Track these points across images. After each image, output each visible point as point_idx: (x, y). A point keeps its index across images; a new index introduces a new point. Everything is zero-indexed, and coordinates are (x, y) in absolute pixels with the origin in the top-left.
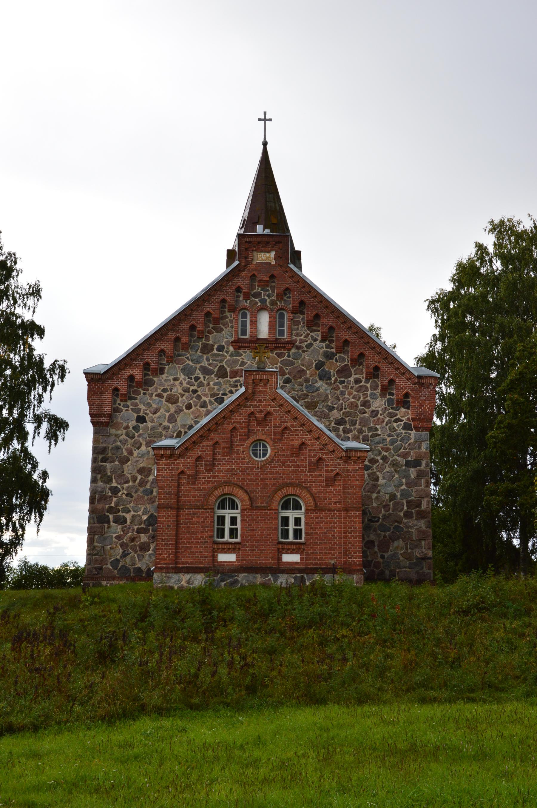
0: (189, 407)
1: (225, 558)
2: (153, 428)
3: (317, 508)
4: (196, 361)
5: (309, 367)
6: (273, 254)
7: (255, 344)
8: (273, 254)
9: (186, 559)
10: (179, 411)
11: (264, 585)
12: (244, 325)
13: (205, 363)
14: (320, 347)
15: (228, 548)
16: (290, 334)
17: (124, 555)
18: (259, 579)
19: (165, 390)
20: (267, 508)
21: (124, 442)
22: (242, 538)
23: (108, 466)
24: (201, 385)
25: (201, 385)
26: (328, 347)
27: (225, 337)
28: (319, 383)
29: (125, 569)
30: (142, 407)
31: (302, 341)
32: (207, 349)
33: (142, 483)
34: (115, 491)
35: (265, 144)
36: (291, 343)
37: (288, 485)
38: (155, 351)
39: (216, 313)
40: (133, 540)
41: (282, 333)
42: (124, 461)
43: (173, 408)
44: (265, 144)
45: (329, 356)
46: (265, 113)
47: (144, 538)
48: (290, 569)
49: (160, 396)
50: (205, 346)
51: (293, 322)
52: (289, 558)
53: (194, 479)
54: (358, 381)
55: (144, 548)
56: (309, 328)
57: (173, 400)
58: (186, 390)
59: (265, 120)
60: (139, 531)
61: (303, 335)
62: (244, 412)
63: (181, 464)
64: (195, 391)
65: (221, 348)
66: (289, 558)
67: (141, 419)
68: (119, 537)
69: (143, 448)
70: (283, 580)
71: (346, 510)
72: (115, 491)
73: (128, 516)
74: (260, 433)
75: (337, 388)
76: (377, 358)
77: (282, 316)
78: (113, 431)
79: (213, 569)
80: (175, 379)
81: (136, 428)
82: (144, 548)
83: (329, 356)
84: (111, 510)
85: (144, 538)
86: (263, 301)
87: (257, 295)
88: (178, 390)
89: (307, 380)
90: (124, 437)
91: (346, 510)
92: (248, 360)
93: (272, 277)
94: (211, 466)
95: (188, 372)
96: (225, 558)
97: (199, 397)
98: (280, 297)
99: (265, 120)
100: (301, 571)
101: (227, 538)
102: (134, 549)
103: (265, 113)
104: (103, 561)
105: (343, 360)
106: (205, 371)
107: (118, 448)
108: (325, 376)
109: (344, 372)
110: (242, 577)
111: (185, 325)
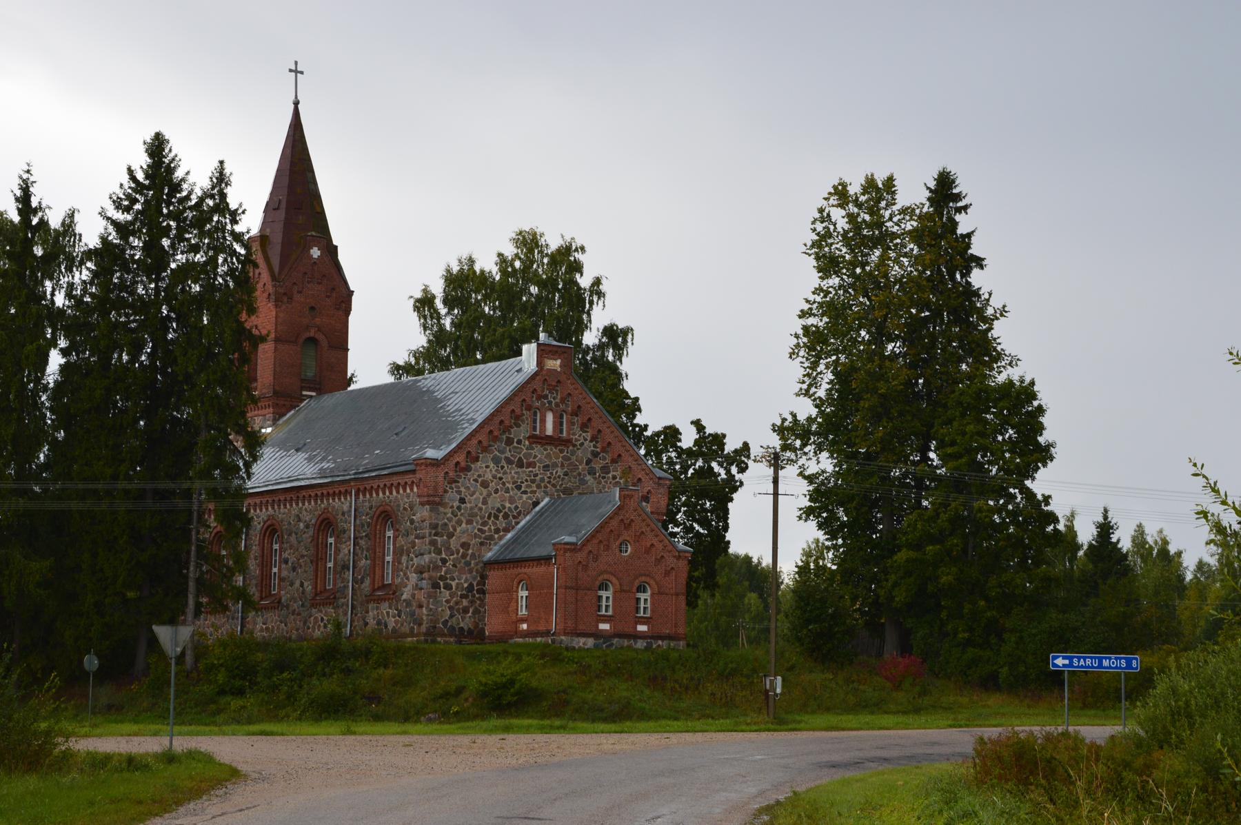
0: (496, 491)
1: (604, 626)
2: (471, 508)
3: (660, 593)
4: (502, 452)
5: (581, 463)
6: (559, 362)
7: (539, 440)
8: (559, 362)
9: (581, 627)
10: (489, 495)
11: (630, 647)
12: (535, 421)
13: (508, 454)
14: (589, 446)
15: (605, 619)
16: (568, 433)
17: (452, 616)
18: (626, 643)
19: (479, 476)
20: (629, 591)
21: (450, 520)
22: (614, 610)
23: (439, 539)
24: (505, 473)
25: (505, 473)
26: (595, 446)
27: (522, 432)
28: (588, 477)
29: (453, 628)
30: (462, 489)
31: (577, 440)
32: (509, 442)
33: (464, 556)
34: (444, 561)
35: (296, 103)
36: (568, 442)
37: (641, 575)
38: (474, 441)
39: (518, 411)
40: (457, 603)
41: (561, 431)
42: (451, 535)
43: (485, 492)
44: (296, 103)
45: (595, 454)
46: (296, 63)
47: (465, 603)
48: (642, 636)
49: (476, 481)
50: (508, 438)
51: (571, 423)
52: (642, 628)
53: (585, 568)
54: (614, 477)
55: (466, 610)
56: (581, 429)
57: (485, 485)
58: (494, 477)
59: (296, 72)
60: (462, 596)
61: (578, 436)
62: (618, 519)
63: (580, 556)
64: (501, 479)
65: (519, 442)
66: (642, 628)
67: (462, 501)
68: (447, 601)
69: (464, 525)
70: (641, 644)
71: (677, 595)
72: (444, 561)
73: (454, 584)
74: (625, 535)
75: (599, 483)
76: (630, 459)
77: (561, 417)
78: (441, 509)
79: (597, 635)
80: (487, 467)
81: (459, 508)
82: (466, 610)
83: (595, 454)
84: (441, 578)
85: (465, 603)
86: (550, 403)
87: (546, 397)
88: (489, 476)
89: (579, 474)
90: (449, 515)
91: (677, 595)
92: (539, 452)
93: (559, 382)
94: (596, 559)
95: (496, 461)
96: (604, 626)
97: (504, 484)
98: (563, 400)
99: (296, 72)
100: (652, 637)
101: (603, 612)
102: (458, 610)
103: (296, 63)
104: (437, 621)
105: (604, 459)
106: (509, 461)
107: (446, 524)
108: (592, 472)
109: (605, 470)
110: (615, 641)
111: (497, 420)
